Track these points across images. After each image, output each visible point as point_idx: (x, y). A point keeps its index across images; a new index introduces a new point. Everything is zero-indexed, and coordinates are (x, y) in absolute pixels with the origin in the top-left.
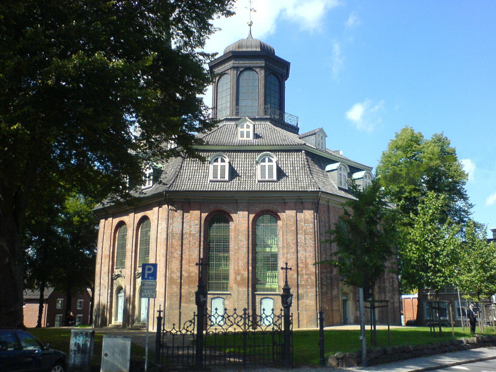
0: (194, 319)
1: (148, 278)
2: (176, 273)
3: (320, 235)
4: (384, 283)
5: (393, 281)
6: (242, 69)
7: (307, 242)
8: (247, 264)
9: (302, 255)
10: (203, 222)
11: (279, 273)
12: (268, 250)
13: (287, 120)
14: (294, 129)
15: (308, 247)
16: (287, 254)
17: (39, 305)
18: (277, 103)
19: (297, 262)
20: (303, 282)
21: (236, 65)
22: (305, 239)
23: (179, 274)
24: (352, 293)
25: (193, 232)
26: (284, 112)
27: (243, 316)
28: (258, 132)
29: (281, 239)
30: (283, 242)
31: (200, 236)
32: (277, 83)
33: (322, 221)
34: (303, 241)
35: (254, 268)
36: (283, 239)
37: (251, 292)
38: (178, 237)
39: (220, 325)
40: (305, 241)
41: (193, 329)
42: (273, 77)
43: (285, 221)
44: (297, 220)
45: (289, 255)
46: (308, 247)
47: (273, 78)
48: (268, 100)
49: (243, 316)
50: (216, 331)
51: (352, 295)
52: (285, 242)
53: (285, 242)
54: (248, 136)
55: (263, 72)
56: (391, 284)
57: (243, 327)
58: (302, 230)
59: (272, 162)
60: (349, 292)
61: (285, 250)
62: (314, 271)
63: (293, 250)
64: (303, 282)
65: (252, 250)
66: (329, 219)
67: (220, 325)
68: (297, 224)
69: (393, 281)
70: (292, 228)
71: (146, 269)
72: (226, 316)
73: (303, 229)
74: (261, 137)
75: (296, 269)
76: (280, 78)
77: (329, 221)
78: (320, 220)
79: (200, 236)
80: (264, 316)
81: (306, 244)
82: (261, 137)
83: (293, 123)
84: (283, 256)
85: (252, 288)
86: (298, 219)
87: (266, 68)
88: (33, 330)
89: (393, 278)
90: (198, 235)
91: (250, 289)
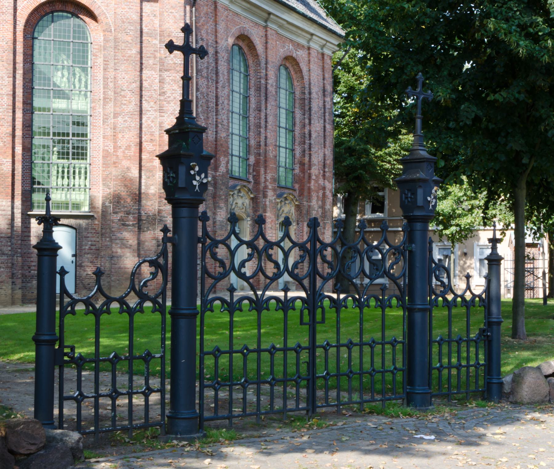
0: (164, 253)
3: (197, 73)
4: (309, 199)
5: (324, 194)
7: (165, 90)
8: (10, 139)
9: (153, 121)
11: (93, 166)
15: (169, 103)
16: (116, 115)
19: (141, 138)
20: (152, 187)
22: (162, 81)
24: (249, 219)
27: (308, 246)
29: (100, 76)
30: (106, 86)
33: (202, 39)
34: (156, 86)
35: (28, 150)
36: (105, 78)
37: (20, 211)
40: (161, 87)
41: (163, 293)
43: (111, 31)
44: (141, 32)
45: (120, 119)
46: (169, 103)
49: (308, 246)
50: (232, 297)
51: (249, 223)
52: (111, 85)
53: (111, 85)
56: (320, 203)
58: (155, 57)
60: (244, 216)
61: (110, 107)
63: (133, 106)
64: (152, 187)
65: (24, 103)
66: (216, 36)
68: (141, 42)
69: (324, 194)
70: (129, 52)
72: (261, 243)
73: (158, 55)
75: (138, 155)
77: (216, 42)
78: (199, 37)
81: (162, 94)
84: (104, 122)
85: (23, 202)
86: (145, 30)
88: (412, 107)
89: (324, 188)
91: (18, 203)
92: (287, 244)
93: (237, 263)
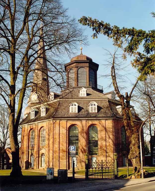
1: (72, 151)
2: (57, 148)
6: (80, 67)
10: (67, 129)
12: (93, 139)
13: (98, 87)
14: (101, 91)
17: (10, 162)
18: (94, 80)
21: (77, 66)
23: (58, 149)
25: (64, 133)
26: (97, 85)
28: (88, 92)
31: (67, 134)
32: (94, 73)
38: (58, 135)
39: (100, 166)
42: (92, 70)
47: (92, 71)
48: (90, 80)
54: (84, 95)
55: (88, 68)
57: (101, 166)
59: (95, 105)
62: (113, 147)
67: (100, 166)
71: (71, 148)
74: (90, 94)
76: (95, 71)
79: (67, 134)
80: (108, 162)
82: (90, 94)
83: (101, 89)
87: (90, 67)
90: (66, 134)
92: (111, 162)
93: (99, 164)
